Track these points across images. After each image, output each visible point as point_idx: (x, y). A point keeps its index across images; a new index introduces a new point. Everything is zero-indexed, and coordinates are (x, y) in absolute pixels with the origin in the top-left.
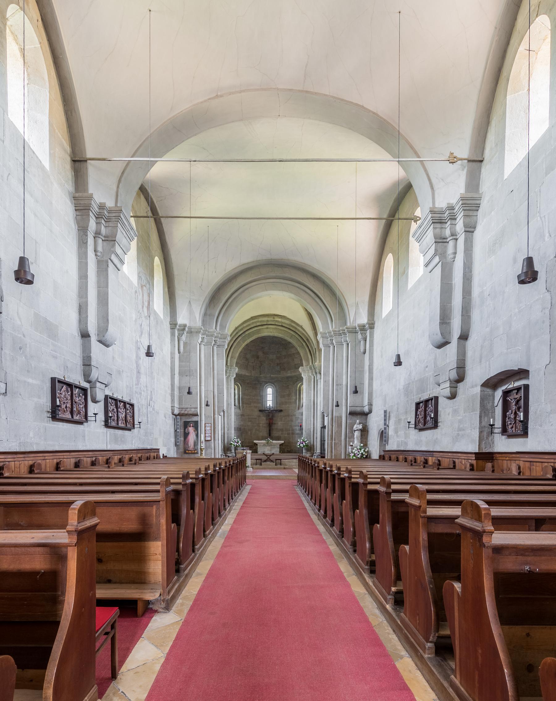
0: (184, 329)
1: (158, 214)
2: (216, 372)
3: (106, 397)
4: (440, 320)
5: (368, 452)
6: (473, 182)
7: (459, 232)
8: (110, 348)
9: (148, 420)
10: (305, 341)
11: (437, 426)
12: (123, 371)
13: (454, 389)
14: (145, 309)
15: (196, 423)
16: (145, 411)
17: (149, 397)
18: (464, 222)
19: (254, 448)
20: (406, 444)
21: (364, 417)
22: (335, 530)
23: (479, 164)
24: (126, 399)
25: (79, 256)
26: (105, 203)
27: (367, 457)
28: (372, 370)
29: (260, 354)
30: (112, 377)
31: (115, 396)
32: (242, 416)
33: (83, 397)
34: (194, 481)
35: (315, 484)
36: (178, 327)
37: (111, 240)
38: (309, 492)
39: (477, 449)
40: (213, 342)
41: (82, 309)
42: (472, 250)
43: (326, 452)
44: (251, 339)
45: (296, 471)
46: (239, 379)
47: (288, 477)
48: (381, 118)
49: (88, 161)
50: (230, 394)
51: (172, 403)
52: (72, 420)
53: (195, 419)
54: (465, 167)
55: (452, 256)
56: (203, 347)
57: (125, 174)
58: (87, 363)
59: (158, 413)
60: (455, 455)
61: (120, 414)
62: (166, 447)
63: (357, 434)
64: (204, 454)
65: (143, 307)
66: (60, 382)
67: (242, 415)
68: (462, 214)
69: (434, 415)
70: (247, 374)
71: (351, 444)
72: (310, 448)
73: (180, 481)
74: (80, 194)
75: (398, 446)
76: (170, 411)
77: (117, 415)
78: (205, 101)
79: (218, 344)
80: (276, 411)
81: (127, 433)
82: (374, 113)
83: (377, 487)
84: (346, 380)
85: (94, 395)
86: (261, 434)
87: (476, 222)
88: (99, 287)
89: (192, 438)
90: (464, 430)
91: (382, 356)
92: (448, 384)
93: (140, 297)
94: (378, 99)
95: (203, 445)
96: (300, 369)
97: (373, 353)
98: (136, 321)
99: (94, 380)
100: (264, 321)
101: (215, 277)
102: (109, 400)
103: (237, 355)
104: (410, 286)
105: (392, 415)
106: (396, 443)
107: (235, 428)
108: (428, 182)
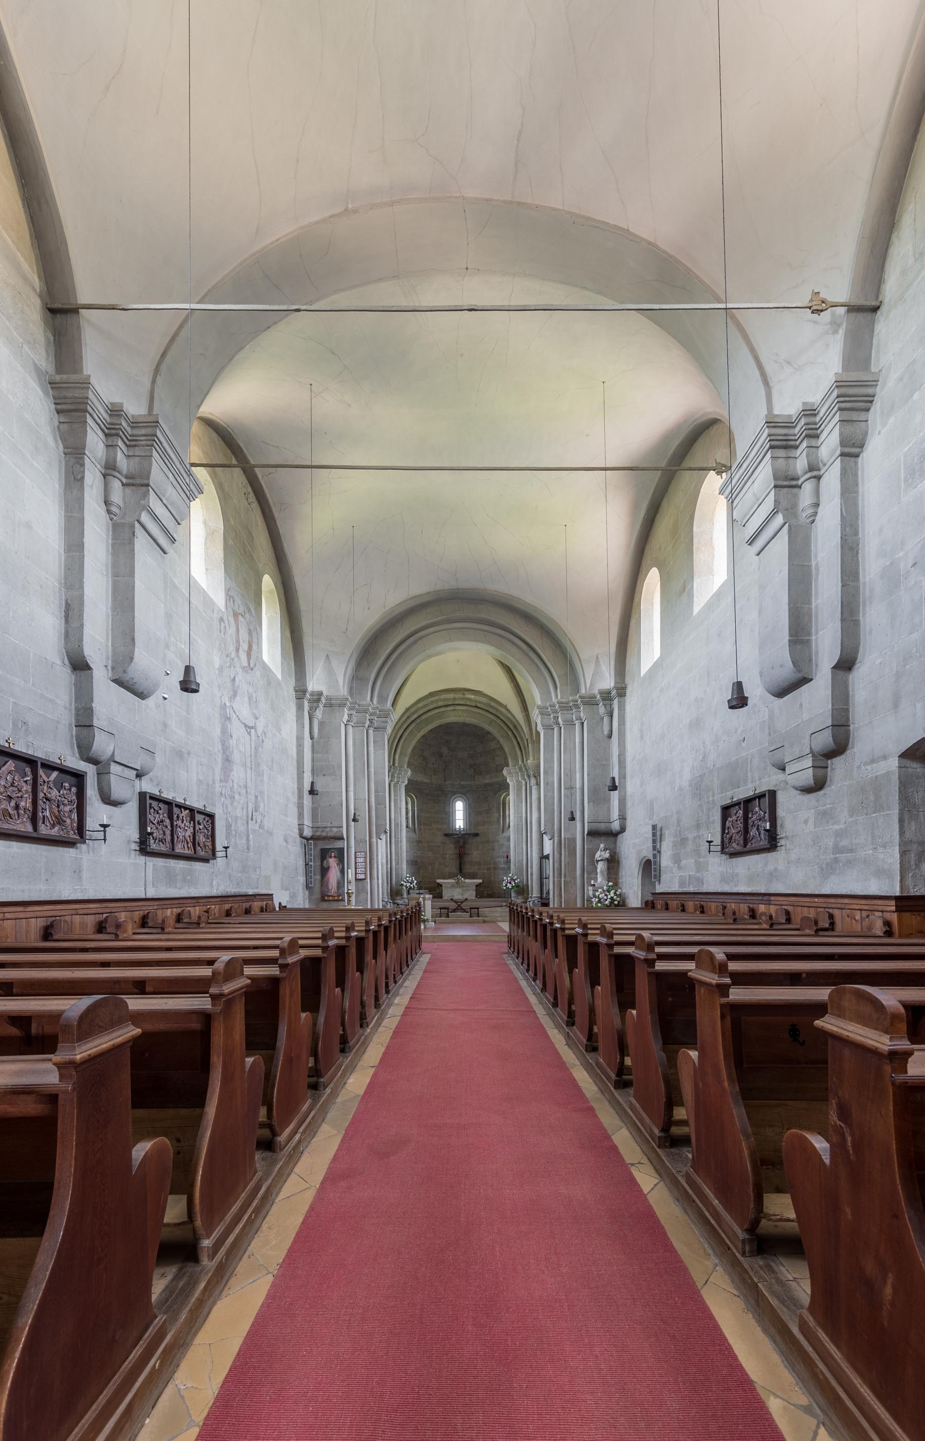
0: (319, 700)
1: (247, 462)
2: (372, 770)
3: (142, 796)
4: (791, 635)
5: (620, 895)
6: (859, 350)
7: (825, 460)
8: (151, 702)
9: (248, 845)
10: (511, 728)
11: (776, 846)
12: (189, 753)
13: (820, 772)
14: (243, 656)
15: (341, 851)
16: (242, 829)
17: (251, 806)
18: (841, 434)
19: (436, 892)
20: (700, 881)
21: (612, 839)
22: (561, 1014)
23: (868, 316)
24: (197, 804)
25: (66, 506)
26: (122, 404)
27: (620, 904)
28: (625, 762)
29: (445, 750)
30: (154, 758)
31: (168, 795)
32: (418, 843)
33: (74, 790)
34: (343, 942)
35: (534, 947)
36: (308, 695)
37: (138, 483)
38: (537, 972)
39: (898, 889)
40: (368, 723)
41: (72, 612)
42: (857, 492)
43: (551, 896)
44: (430, 727)
45: (505, 926)
46: (413, 788)
47: (493, 938)
48: (664, 251)
49: (83, 312)
50: (400, 810)
51: (299, 819)
52: (35, 835)
53: (338, 844)
54: (839, 326)
55: (810, 511)
56: (350, 729)
57: (168, 359)
58: (84, 722)
59: (270, 834)
60: (832, 900)
61: (176, 828)
62: (287, 888)
63: (601, 866)
64: (353, 902)
65: (237, 650)
66: (153, 798)
67: (419, 842)
68: (837, 418)
69: (771, 826)
70: (425, 781)
71: (592, 882)
72: (522, 890)
73: (319, 942)
74: (65, 377)
75: (682, 883)
76: (297, 831)
77: (172, 831)
78: (324, 220)
79: (376, 725)
80: (469, 834)
81: (198, 866)
82: (650, 243)
83: (630, 950)
84: (582, 779)
85: (106, 789)
86: (447, 870)
87: (866, 434)
88: (115, 575)
89: (334, 875)
90: (851, 851)
91: (642, 738)
92: (808, 762)
93: (232, 631)
94: (656, 211)
95: (352, 888)
96: (505, 772)
97: (624, 735)
98: (221, 669)
99: (104, 758)
100: (448, 699)
101: (368, 617)
102: (149, 801)
103: (410, 750)
104: (696, 609)
105: (666, 832)
106: (677, 880)
107: (407, 861)
108: (757, 373)
